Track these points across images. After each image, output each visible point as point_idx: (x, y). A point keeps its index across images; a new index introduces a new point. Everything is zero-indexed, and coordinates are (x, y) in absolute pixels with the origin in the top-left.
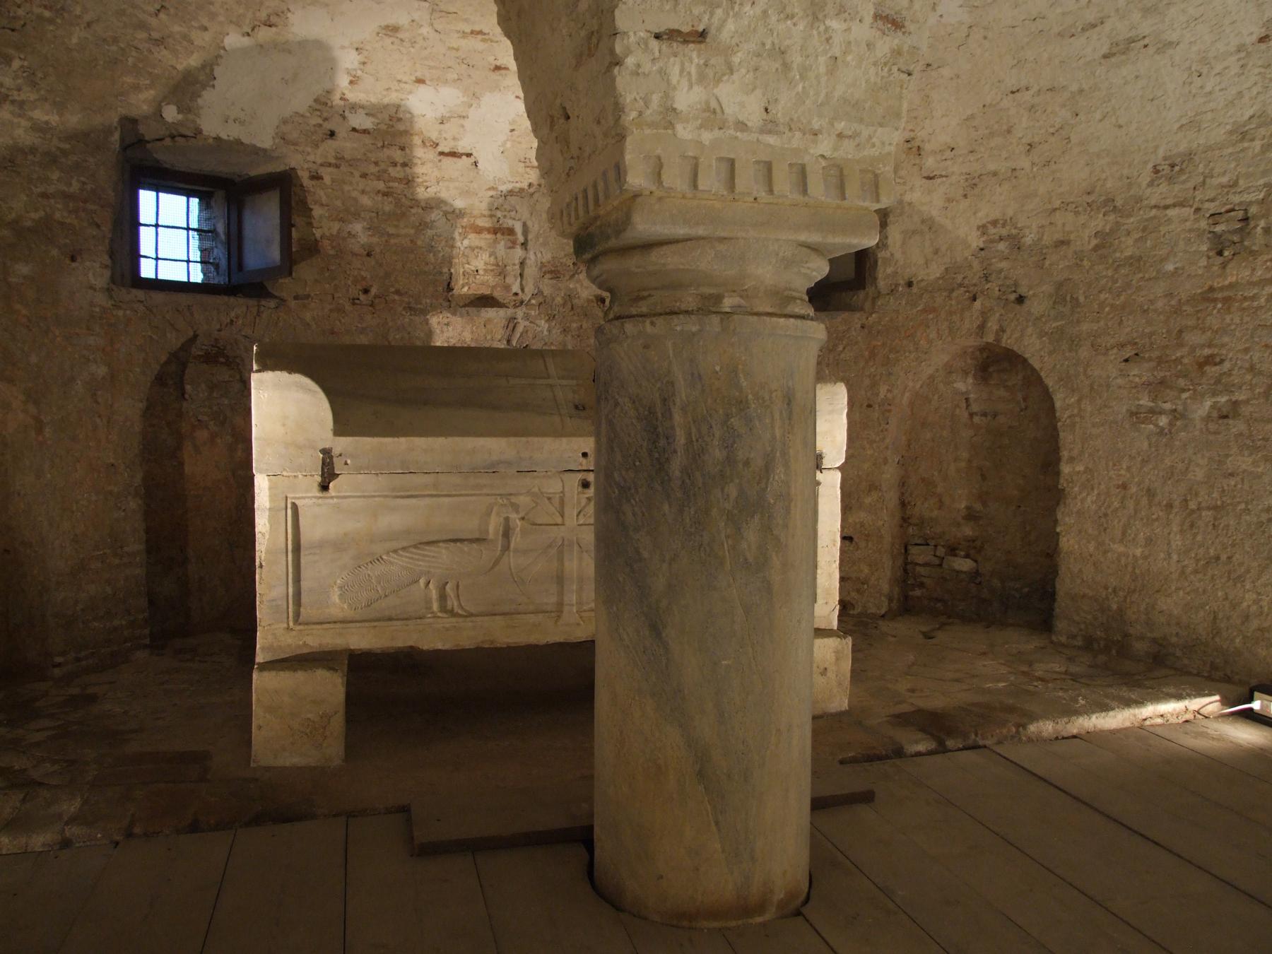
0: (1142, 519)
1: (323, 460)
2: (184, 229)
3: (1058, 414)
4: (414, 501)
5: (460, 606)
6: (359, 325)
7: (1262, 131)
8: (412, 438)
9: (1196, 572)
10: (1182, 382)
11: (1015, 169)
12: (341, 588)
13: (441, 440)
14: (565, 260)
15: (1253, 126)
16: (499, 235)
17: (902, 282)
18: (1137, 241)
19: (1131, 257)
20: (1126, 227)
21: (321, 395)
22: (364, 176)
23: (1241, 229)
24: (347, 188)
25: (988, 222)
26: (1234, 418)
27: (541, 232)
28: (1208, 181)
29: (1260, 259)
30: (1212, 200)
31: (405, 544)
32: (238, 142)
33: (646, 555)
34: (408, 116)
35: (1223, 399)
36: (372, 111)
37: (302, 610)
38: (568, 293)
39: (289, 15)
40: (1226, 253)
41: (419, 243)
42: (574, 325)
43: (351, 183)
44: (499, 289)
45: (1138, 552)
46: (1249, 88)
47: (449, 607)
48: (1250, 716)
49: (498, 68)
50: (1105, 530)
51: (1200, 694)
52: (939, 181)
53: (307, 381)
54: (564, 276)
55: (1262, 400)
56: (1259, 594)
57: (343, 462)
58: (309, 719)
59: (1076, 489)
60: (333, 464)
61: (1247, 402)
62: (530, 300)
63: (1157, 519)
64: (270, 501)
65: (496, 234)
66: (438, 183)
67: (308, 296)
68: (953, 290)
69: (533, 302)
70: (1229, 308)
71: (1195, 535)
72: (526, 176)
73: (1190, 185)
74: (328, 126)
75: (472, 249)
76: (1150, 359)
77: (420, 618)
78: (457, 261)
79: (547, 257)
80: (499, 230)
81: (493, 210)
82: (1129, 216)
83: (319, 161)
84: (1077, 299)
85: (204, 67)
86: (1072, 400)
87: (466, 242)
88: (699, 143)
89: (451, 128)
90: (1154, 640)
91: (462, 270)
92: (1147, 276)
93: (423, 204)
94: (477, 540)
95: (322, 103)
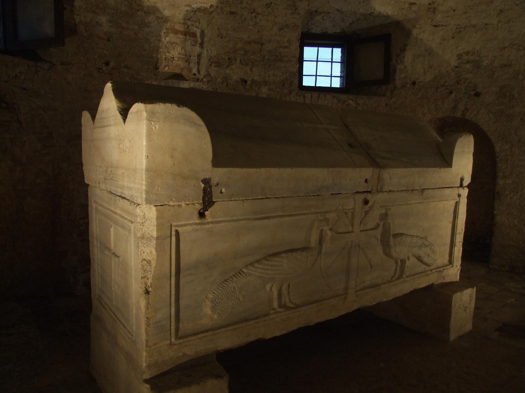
1: (205, 190)
2: (331, 74)
4: (266, 222)
8: (269, 169)
11: (487, 24)
12: (212, 301)
14: (224, 56)
16: (188, 37)
17: (409, 82)
21: (204, 129)
25: (464, 53)
27: (212, 37)
37: (181, 325)
44: (186, 70)
47: (283, 303)
52: (440, 28)
53: (193, 115)
57: (219, 191)
59: (507, 192)
60: (212, 192)
62: (203, 79)
64: (158, 230)
65: (186, 36)
68: (438, 88)
69: (205, 80)
75: (172, 43)
78: (161, 50)
80: (188, 33)
81: (186, 19)
86: (507, 147)
87: (168, 39)
91: (164, 56)
94: (304, 249)
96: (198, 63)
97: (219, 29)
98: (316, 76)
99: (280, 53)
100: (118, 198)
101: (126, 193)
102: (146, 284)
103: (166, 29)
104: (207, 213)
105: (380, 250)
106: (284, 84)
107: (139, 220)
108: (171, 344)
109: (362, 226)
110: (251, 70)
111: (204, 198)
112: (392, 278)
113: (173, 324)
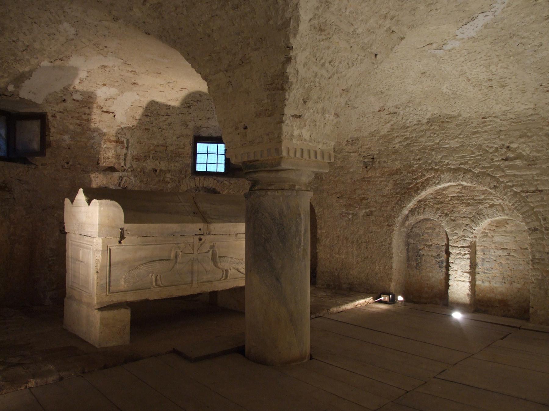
0: (344, 247)
3: (316, 214)
4: (148, 246)
5: (162, 283)
6: (65, 177)
7: (378, 135)
9: (361, 262)
10: (355, 205)
12: (125, 279)
13: (158, 225)
15: (375, 133)
16: (118, 144)
18: (341, 162)
19: (339, 166)
20: (338, 157)
21: (121, 209)
22: (73, 117)
23: (372, 162)
24: (65, 121)
26: (371, 216)
28: (363, 146)
29: (378, 171)
30: (364, 152)
31: (145, 262)
32: (30, 101)
33: (274, 258)
34: (95, 96)
35: (368, 210)
36: (83, 93)
37: (111, 288)
38: (143, 167)
39: (71, 57)
40: (368, 168)
41: (88, 145)
42: (145, 179)
43: (67, 120)
45: (343, 257)
46: (375, 123)
47: (158, 284)
48: (381, 302)
49: (134, 83)
50: (333, 250)
51: (367, 297)
53: (116, 203)
54: (141, 160)
55: (379, 211)
56: (380, 267)
58: (119, 328)
59: (323, 238)
61: (375, 211)
62: (128, 169)
63: (349, 246)
65: (117, 143)
66: (99, 122)
67: (46, 164)
69: (129, 170)
70: (369, 184)
71: (361, 251)
72: (132, 122)
73: (358, 147)
74: (64, 97)
75: (108, 148)
76: (346, 198)
77: (149, 288)
79: (135, 153)
80: (118, 142)
81: (117, 133)
82: (339, 154)
83: (57, 110)
84: (322, 178)
85: (29, 72)
87: (105, 146)
88: (297, 144)
89: (109, 103)
90: (349, 284)
91: (103, 156)
92: (345, 172)
93: (92, 130)
94: (168, 260)
95: (66, 89)
96: (125, 160)
97: (138, 139)
98: (207, 163)
99: (179, 152)
100: (85, 236)
101: (89, 234)
102: (97, 269)
103: (105, 140)
104: (122, 242)
105: (211, 264)
106: (181, 171)
107: (95, 244)
108: (107, 295)
109: (199, 251)
110: (159, 163)
111: (121, 235)
112: (220, 279)
113: (108, 286)
